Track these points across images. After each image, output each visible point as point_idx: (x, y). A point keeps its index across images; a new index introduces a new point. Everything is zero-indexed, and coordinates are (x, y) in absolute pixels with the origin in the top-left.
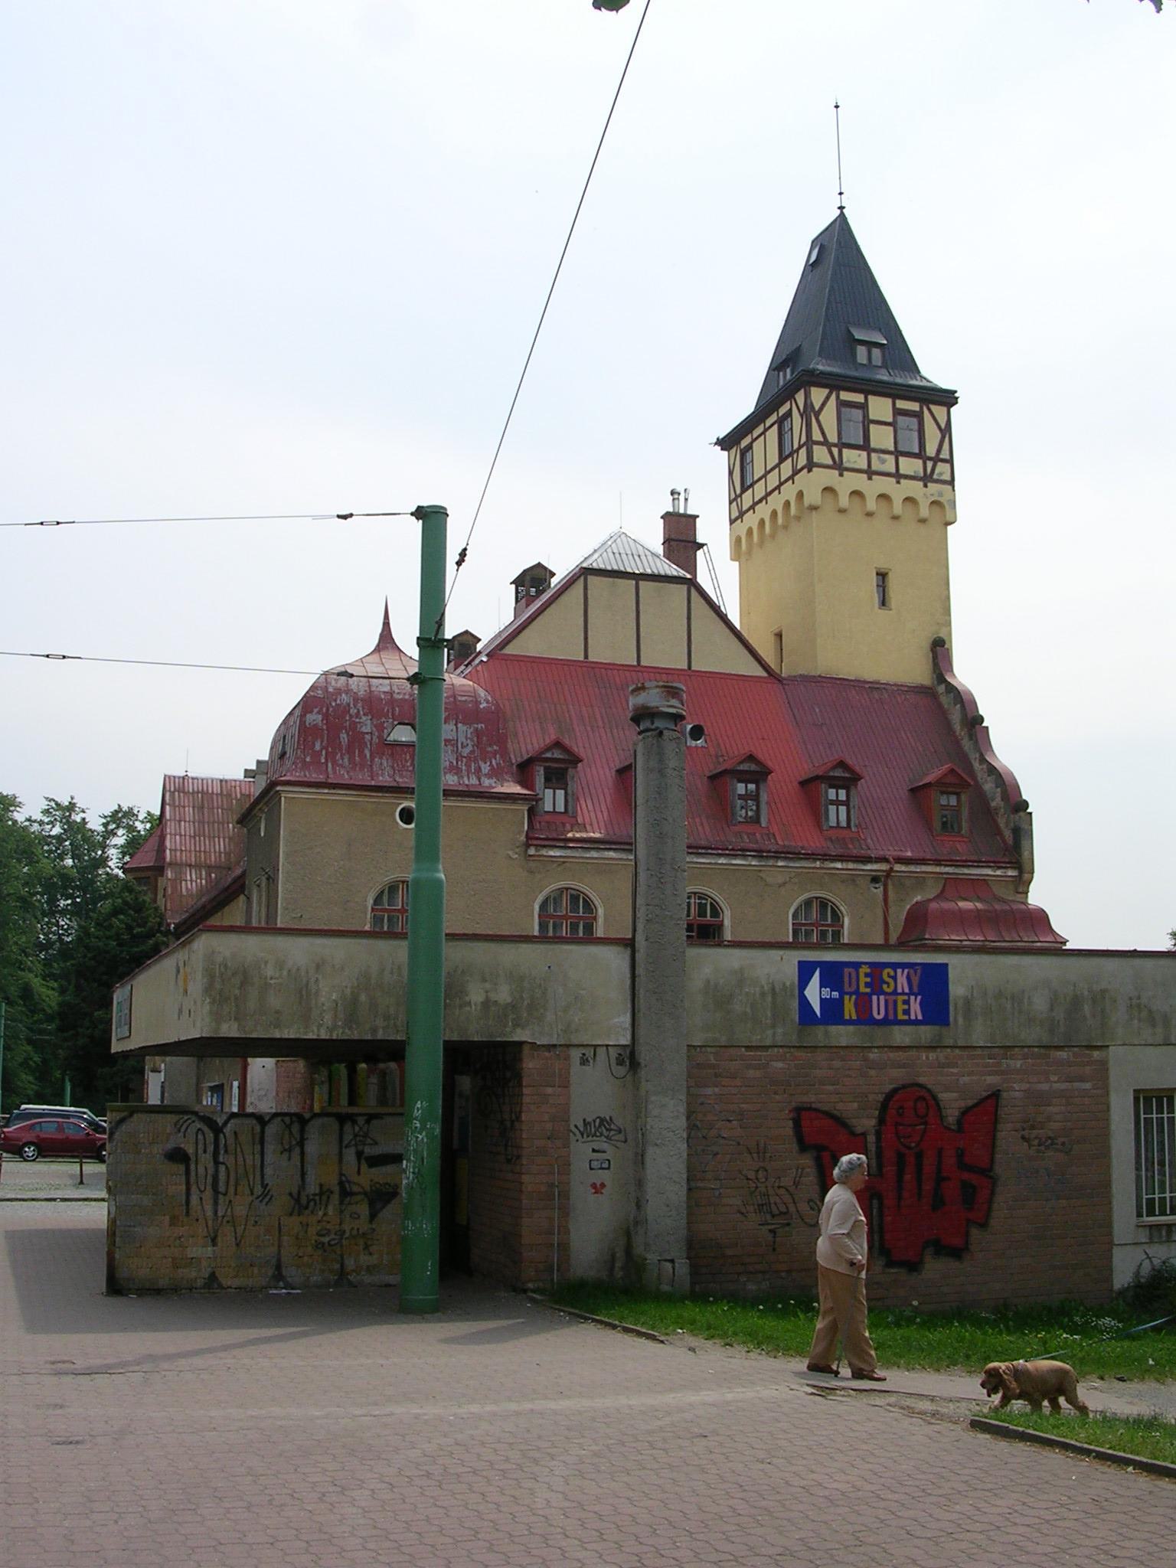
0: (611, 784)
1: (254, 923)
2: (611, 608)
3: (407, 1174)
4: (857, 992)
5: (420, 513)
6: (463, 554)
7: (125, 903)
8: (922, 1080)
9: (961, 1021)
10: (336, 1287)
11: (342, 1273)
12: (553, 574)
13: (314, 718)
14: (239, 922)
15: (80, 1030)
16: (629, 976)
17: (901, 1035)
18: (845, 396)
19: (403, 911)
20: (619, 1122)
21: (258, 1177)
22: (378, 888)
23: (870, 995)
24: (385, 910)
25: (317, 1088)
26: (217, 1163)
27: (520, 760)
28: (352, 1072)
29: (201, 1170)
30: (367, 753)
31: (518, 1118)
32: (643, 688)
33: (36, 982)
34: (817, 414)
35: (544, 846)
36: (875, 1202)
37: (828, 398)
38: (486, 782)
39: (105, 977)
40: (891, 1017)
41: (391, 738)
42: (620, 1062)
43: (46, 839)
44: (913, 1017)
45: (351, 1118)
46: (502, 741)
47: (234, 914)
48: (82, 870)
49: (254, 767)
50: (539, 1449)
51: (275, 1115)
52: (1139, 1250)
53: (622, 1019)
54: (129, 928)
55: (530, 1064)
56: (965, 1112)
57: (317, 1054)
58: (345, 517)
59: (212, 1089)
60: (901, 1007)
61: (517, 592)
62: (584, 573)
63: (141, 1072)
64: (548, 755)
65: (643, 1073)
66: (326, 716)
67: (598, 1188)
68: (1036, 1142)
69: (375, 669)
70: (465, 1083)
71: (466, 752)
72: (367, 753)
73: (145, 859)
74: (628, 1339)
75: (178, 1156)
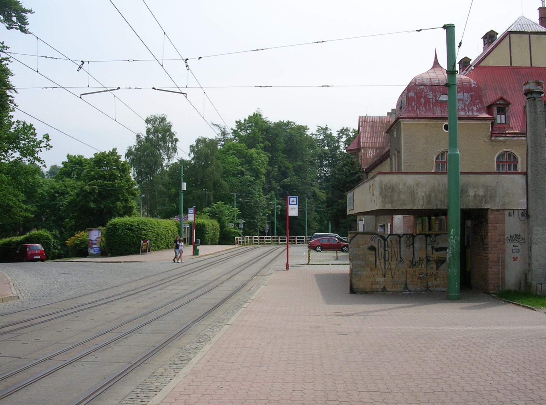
0: (522, 112)
1: (393, 171)
2: (520, 45)
3: (449, 254)
5: (445, 27)
6: (460, 44)
7: (348, 162)
10: (425, 291)
11: (427, 287)
12: (497, 34)
13: (412, 94)
14: (388, 171)
15: (334, 207)
16: (525, 185)
19: (446, 162)
20: (522, 236)
21: (399, 256)
22: (437, 154)
25: (418, 226)
26: (385, 251)
27: (487, 105)
28: (430, 219)
29: (380, 253)
30: (431, 105)
31: (487, 235)
32: (528, 83)
33: (317, 191)
35: (498, 136)
38: (475, 114)
39: (342, 188)
41: (440, 99)
42: (523, 215)
43: (318, 141)
45: (430, 235)
46: (480, 98)
47: (385, 167)
48: (331, 151)
49: (391, 111)
50: (490, 340)
51: (404, 234)
53: (523, 200)
54: (349, 171)
55: (491, 216)
57: (417, 214)
58: (419, 31)
59: (381, 226)
61: (484, 41)
62: (509, 33)
63: (356, 221)
64: (498, 102)
65: (531, 219)
66: (416, 93)
67: (515, 259)
69: (432, 75)
70: (469, 223)
71: (467, 103)
72: (431, 105)
73: (354, 146)
74: (524, 309)
75: (372, 248)
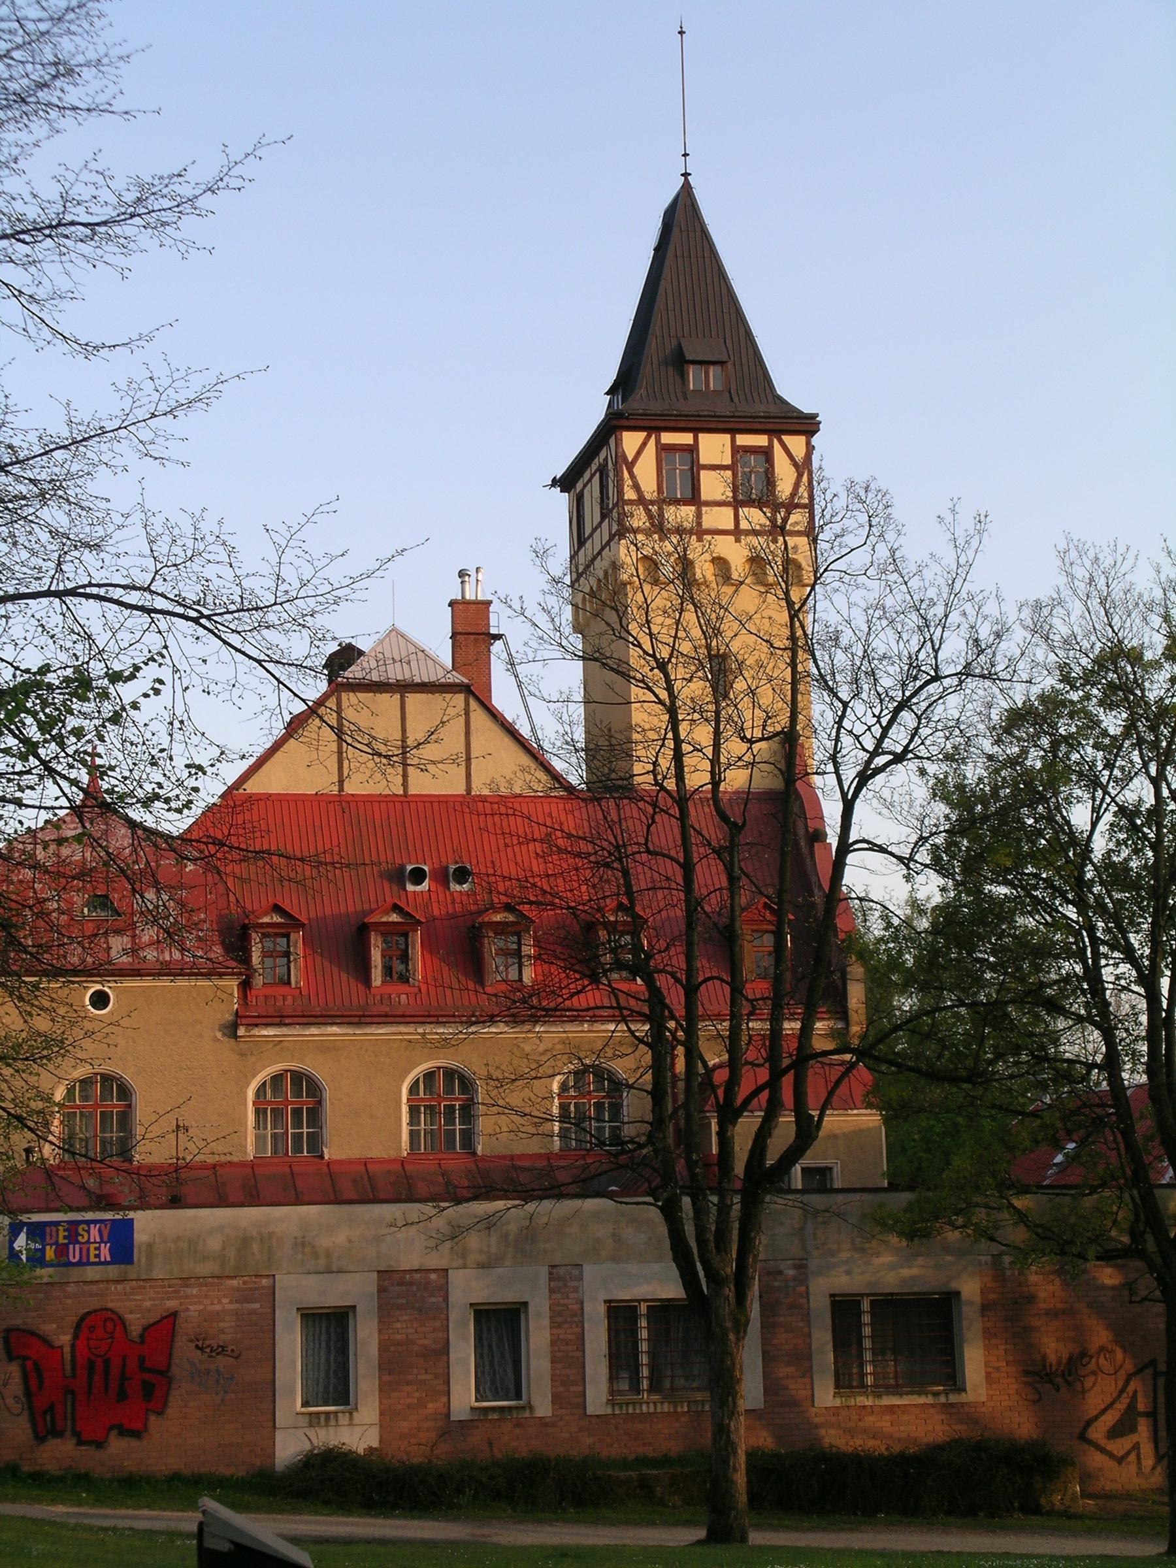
4: (56, 1243)
8: (110, 1305)
9: (143, 1260)
17: (92, 1273)
18: (668, 438)
23: (66, 1245)
24: (78, 1107)
34: (630, 466)
35: (256, 1025)
36: (69, 1397)
37: (644, 444)
40: (85, 1260)
44: (103, 1259)
52: (300, 1433)
56: (146, 1329)
60: (92, 1252)
68: (208, 1350)
